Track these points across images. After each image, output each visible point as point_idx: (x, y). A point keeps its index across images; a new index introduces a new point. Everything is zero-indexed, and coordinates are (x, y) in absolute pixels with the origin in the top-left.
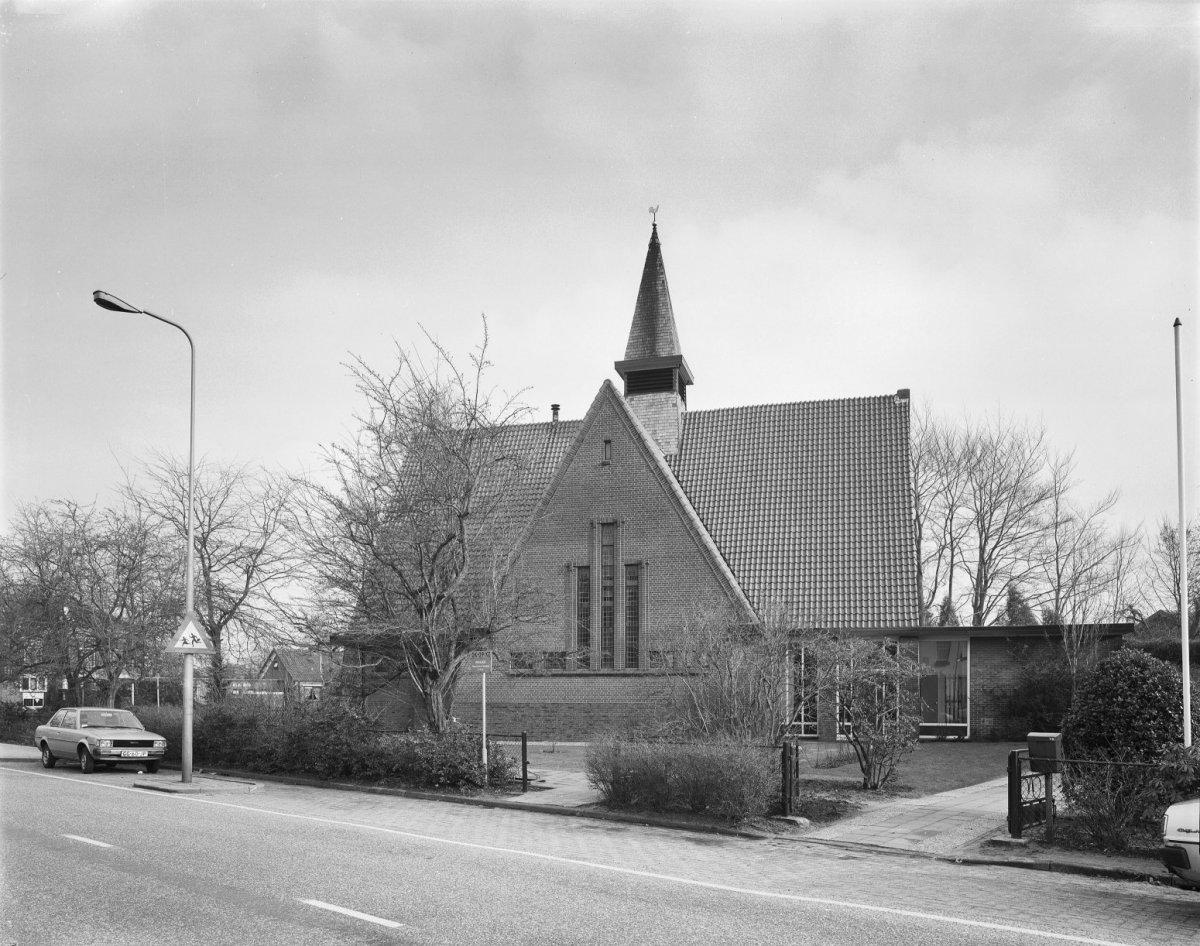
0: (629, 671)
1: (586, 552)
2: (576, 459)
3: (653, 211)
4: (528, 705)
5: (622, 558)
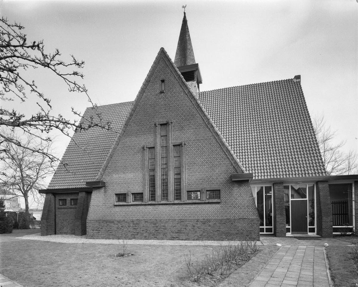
0: (176, 202)
1: (152, 140)
2: (146, 91)
4: (124, 220)
5: (172, 141)
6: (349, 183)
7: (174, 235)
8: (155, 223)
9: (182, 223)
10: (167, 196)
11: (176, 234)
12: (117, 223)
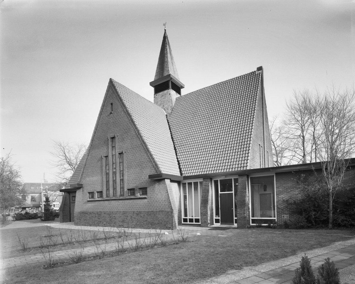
3: (164, 25)
4: (93, 212)
6: (272, 175)
7: (121, 224)
8: (110, 214)
9: (125, 214)
10: (32, 199)
11: (122, 223)
12: (89, 214)
